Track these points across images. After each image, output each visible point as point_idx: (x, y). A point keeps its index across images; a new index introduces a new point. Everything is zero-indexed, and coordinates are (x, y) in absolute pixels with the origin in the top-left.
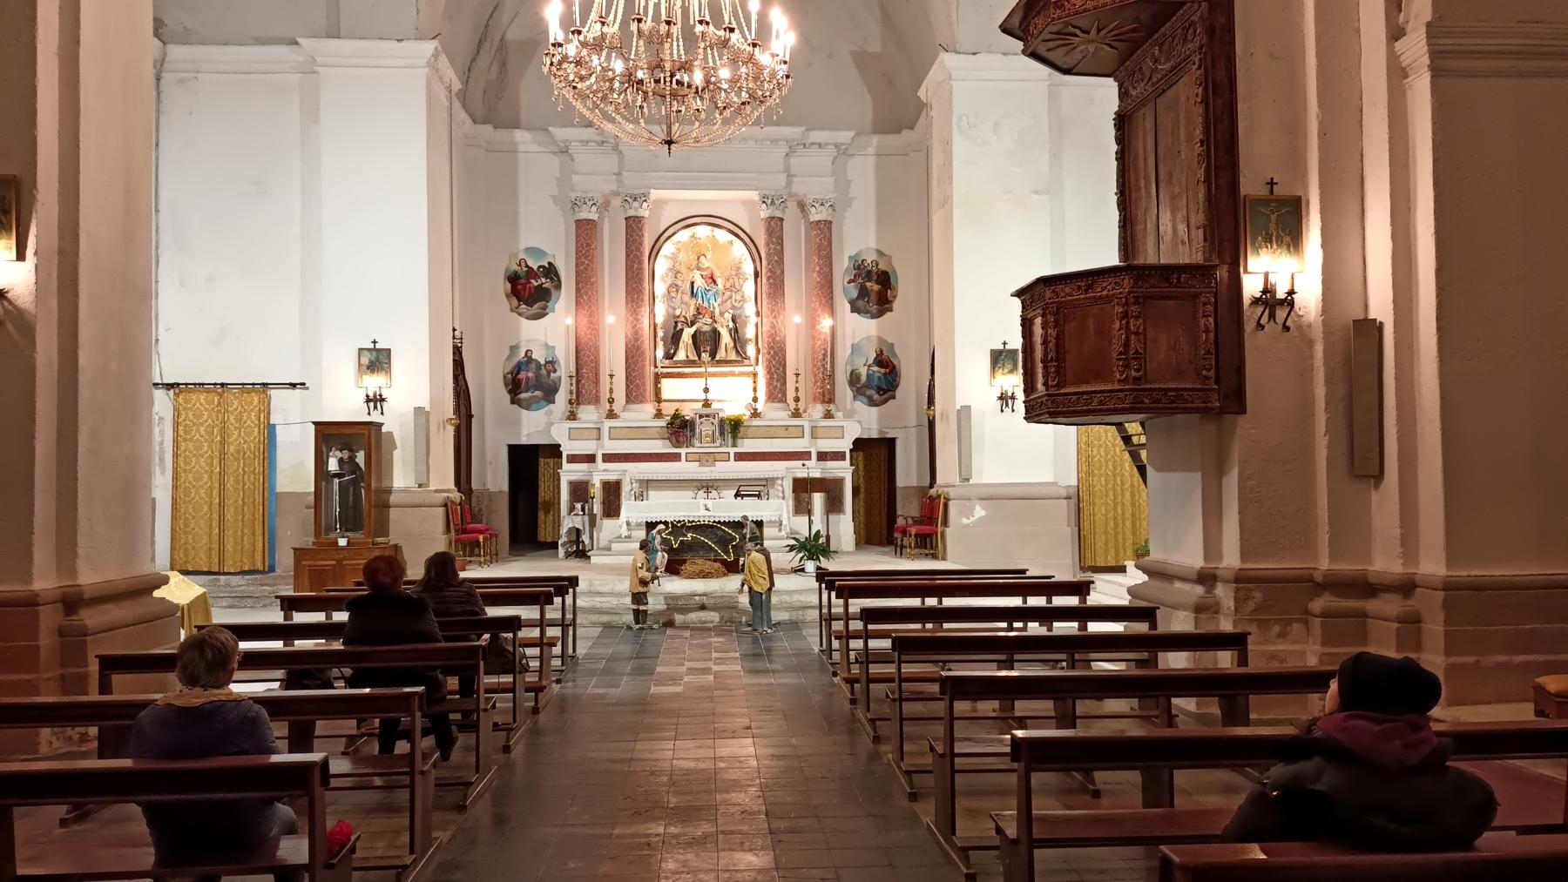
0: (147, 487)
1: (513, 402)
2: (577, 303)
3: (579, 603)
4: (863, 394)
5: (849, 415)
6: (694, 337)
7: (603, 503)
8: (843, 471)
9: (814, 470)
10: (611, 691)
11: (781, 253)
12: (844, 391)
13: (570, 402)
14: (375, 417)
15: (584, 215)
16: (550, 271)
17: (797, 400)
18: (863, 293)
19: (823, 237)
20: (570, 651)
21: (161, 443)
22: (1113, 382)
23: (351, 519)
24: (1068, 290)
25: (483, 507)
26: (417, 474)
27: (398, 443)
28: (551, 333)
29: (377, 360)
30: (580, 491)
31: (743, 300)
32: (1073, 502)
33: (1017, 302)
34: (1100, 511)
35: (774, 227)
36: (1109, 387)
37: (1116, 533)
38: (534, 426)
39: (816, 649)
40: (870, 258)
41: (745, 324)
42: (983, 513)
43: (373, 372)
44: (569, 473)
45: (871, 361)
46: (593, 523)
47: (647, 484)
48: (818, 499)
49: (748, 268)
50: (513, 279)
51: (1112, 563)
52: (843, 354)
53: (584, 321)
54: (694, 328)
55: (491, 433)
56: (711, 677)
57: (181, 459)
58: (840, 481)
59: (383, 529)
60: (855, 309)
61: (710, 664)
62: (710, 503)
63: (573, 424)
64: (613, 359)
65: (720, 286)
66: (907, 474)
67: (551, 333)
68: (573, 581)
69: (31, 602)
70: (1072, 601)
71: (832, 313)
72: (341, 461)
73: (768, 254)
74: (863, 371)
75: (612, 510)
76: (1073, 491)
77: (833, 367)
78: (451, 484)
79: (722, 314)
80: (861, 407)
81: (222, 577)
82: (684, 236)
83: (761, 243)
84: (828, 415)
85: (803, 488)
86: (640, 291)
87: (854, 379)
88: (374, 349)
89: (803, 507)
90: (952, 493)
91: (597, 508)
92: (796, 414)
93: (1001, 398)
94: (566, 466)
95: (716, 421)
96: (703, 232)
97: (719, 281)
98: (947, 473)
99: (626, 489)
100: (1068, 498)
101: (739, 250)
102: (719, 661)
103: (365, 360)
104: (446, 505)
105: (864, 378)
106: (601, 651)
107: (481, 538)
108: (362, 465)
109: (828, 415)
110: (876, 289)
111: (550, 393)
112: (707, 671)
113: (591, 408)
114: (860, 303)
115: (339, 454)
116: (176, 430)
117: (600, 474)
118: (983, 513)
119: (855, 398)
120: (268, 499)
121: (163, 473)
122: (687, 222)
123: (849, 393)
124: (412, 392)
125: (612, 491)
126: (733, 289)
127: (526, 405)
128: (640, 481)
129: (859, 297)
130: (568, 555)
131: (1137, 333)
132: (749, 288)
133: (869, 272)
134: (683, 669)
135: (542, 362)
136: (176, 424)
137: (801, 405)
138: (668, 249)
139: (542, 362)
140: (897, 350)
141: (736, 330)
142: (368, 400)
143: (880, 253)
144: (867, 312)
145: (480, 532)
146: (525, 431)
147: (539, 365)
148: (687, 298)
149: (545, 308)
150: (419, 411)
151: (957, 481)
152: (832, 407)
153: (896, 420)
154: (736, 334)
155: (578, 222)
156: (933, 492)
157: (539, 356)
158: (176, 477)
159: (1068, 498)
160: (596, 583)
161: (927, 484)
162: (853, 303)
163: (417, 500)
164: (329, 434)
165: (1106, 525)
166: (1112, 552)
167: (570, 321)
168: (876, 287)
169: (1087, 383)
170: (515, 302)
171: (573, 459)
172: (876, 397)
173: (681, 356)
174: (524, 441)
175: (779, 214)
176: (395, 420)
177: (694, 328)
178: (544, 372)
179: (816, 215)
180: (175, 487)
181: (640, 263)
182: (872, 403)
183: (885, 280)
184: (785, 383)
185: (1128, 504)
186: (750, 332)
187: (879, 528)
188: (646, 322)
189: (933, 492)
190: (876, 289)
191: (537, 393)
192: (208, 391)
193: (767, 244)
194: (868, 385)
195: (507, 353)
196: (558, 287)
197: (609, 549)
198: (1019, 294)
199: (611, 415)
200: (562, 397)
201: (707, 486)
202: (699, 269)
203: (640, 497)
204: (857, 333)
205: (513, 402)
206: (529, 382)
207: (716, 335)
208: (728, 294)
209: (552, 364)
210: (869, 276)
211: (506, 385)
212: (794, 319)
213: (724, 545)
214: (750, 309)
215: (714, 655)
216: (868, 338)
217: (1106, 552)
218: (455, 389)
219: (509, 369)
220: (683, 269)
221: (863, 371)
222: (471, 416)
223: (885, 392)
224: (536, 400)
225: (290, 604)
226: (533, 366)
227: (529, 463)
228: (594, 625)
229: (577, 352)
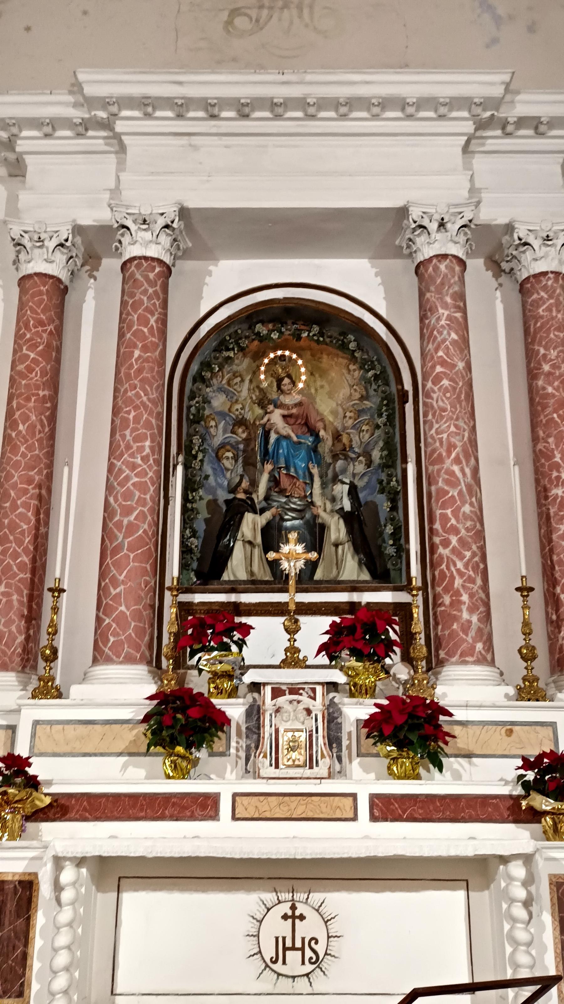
155: (24, 280)
177: (268, 515)
184: (487, 617)
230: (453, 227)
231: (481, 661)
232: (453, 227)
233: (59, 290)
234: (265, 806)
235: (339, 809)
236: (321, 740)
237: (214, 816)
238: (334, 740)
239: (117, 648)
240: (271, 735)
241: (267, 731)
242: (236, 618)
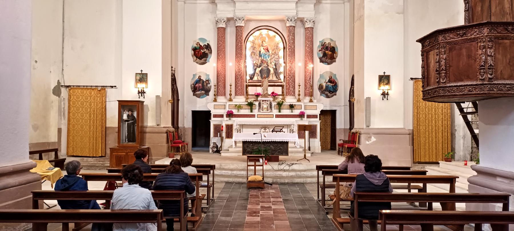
1: (194, 95)
2: (218, 58)
3: (215, 180)
4: (324, 93)
5: (319, 101)
6: (260, 71)
7: (226, 133)
8: (317, 122)
9: (305, 122)
10: (228, 219)
11: (294, 40)
12: (317, 92)
13: (215, 95)
14: (142, 99)
15: (221, 26)
16: (208, 47)
17: (299, 95)
18: (325, 55)
19: (310, 34)
20: (211, 195)
21: (64, 108)
22: (477, 80)
23: (131, 137)
24: (451, 36)
25: (183, 133)
26: (156, 120)
27: (150, 109)
28: (208, 70)
29: (142, 78)
30: (218, 129)
31: (279, 58)
32: (411, 136)
33: (420, 45)
34: (422, 140)
35: (292, 30)
36: (475, 83)
37: (429, 149)
38: (202, 104)
39: (316, 198)
40: (327, 42)
41: (279, 67)
42: (375, 140)
43: (141, 82)
44: (214, 121)
45: (327, 81)
46: (222, 140)
47: (242, 126)
48: (307, 133)
49: (281, 46)
50: (194, 49)
51: (434, 161)
52: (316, 78)
53: (220, 65)
54: (260, 68)
55: (186, 106)
56: (272, 212)
57: (71, 114)
58: (315, 126)
59: (142, 141)
60: (321, 61)
61: (271, 204)
62: (266, 134)
63: (215, 103)
64: (230, 79)
65: (270, 52)
66: (341, 123)
67: (208, 70)
68: (213, 167)
70: (444, 189)
71: (313, 63)
72: (128, 116)
73: (289, 40)
74: (324, 85)
75: (229, 135)
76: (411, 132)
77: (313, 83)
78: (170, 125)
79: (271, 63)
80: (323, 98)
81: (85, 158)
82: (257, 33)
83: (286, 36)
84: (311, 101)
85: (302, 129)
86: (241, 54)
87: (320, 87)
88: (142, 73)
89: (301, 136)
90: (362, 131)
91: (224, 135)
92: (299, 100)
93: (382, 94)
94: (213, 119)
95: (269, 103)
96: (264, 32)
97: (270, 51)
98: (359, 124)
99: (234, 127)
100: (409, 134)
101: (278, 39)
102: (274, 203)
103: (138, 78)
104: (167, 133)
105: (324, 87)
106: (224, 195)
107: (180, 146)
108: (136, 117)
109: (311, 101)
110: (329, 54)
111: (207, 92)
112: (269, 208)
113: (223, 97)
114: (324, 59)
115: (127, 113)
116: (69, 103)
117: (225, 122)
118: (375, 140)
119: (321, 95)
120: (106, 130)
121: (64, 119)
122: (258, 28)
123: (319, 93)
124: (156, 89)
125: (230, 128)
126: (276, 54)
127: (199, 96)
128: (240, 125)
130: (214, 152)
131: (491, 56)
132: (281, 53)
133: (327, 47)
134: (259, 207)
135: (205, 80)
136: (69, 101)
137: (301, 97)
138: (251, 38)
139: (205, 80)
140: (337, 76)
141: (276, 69)
142: (139, 93)
143: (331, 40)
144: (326, 62)
145: (180, 143)
146: (198, 106)
147: (203, 82)
148: (257, 57)
149: (206, 60)
150: (158, 97)
151: (365, 127)
152: (312, 98)
153: (338, 103)
154: (276, 70)
155: (218, 28)
156: (353, 131)
157: (204, 78)
158: (69, 120)
159: (409, 134)
160: (223, 165)
161: (348, 127)
162: (320, 59)
163: (157, 130)
164: (124, 105)
165: (425, 145)
166: (427, 156)
167: (215, 65)
168: (330, 53)
169: (462, 80)
170: (195, 58)
171: (215, 116)
172: (329, 94)
173: (255, 78)
174: (198, 109)
175: (293, 25)
176: (149, 100)
177: (260, 68)
178: (205, 84)
179: (308, 25)
180: (69, 124)
181: (241, 43)
182: (328, 97)
183: (333, 50)
184: (294, 89)
185: (434, 137)
186: (282, 70)
187: (330, 144)
188: (243, 66)
189: (353, 131)
190: (329, 54)
191: (203, 92)
192: (82, 89)
193: (289, 36)
194: (325, 90)
195: (192, 77)
196: (211, 53)
197: (228, 150)
198: (421, 41)
199: (231, 100)
200: (212, 93)
201: (265, 127)
202: (262, 46)
203: (239, 131)
204: (321, 70)
205: (194, 95)
206: (200, 88)
207: (269, 71)
208: (273, 56)
209: (208, 81)
210: (327, 48)
211: (192, 89)
212: (299, 65)
213: (275, 151)
214: (281, 61)
215: (272, 199)
216: (326, 72)
217: (425, 156)
218: (172, 89)
219: (193, 83)
220: (257, 46)
221: (324, 85)
222: (178, 100)
224: (202, 94)
225: (110, 171)
226: (201, 82)
227: (201, 119)
228: (222, 182)
229: (217, 76)
230: (293, 20)
231: (293, 95)
232: (293, 20)
233: (224, 29)
234: (261, 116)
235: (271, 116)
236: (269, 108)
237: (255, 117)
238: (271, 107)
239: (239, 93)
240: (60, 131)
241: (262, 106)
242: (456, 204)
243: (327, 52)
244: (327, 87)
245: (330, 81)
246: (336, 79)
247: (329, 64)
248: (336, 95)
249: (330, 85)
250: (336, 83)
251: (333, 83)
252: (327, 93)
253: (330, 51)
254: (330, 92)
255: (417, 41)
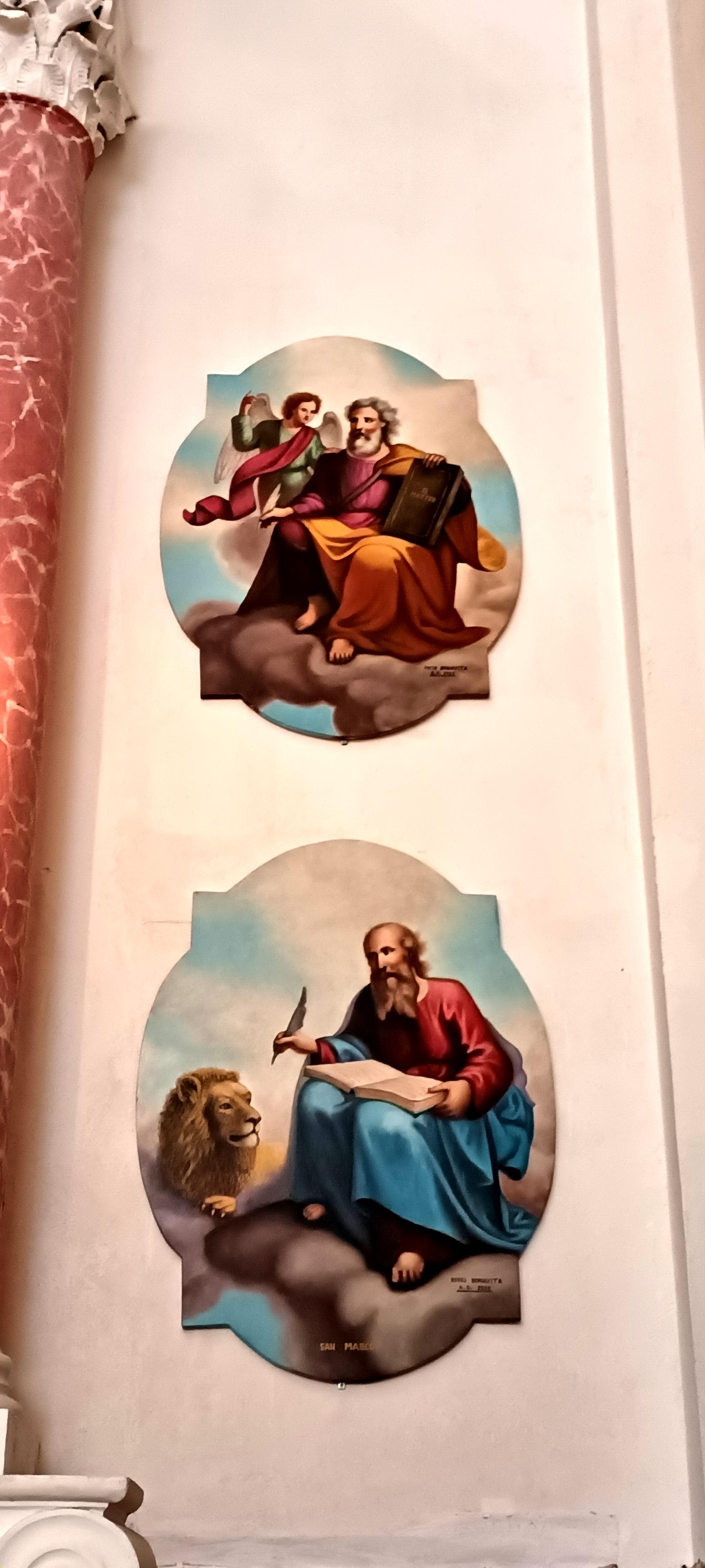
0: (16, 19)
4: (262, 1272)
18: (290, 576)
45: (328, 1018)
60: (231, 675)
69: (24, 219)
74: (271, 1092)
87: (195, 1139)
105: (271, 1145)
114: (271, 640)
119: (534, 1105)
129: (253, 606)
140: (518, 946)
143: (409, 367)
144: (308, 693)
162: (213, 636)
168: (384, 550)
182: (342, 1355)
183: (439, 508)
194: (283, 1209)
210: (332, 482)
221: (271, 1092)
223: (441, 1255)
243: (326, 531)
244: (328, 1138)
245: (392, 1022)
246: (510, 980)
247: (359, 723)
248: (505, 1310)
249: (397, 1098)
250: (506, 1065)
251: (451, 1064)
252: (315, 1257)
253: (381, 520)
254: (380, 1237)
255: (128, 1479)
